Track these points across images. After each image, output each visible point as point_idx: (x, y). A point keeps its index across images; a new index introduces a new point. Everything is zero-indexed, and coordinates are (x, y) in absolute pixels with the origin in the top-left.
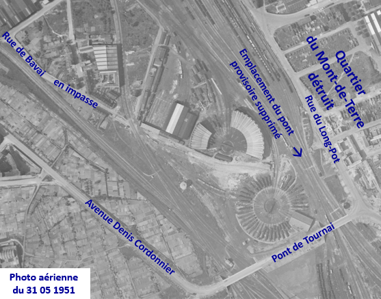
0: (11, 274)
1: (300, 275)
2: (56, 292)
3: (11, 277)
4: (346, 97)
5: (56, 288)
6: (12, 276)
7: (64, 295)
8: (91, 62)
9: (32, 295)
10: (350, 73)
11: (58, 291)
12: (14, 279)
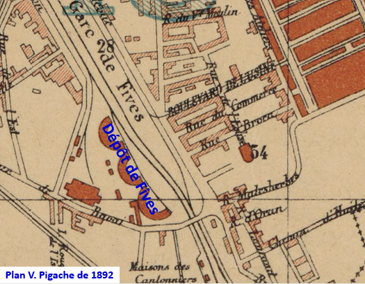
0: (7, 272)
1: (329, 147)
2: (94, 277)
3: (7, 275)
4: (265, 280)
5: (94, 273)
6: (8, 274)
7: (102, 280)
8: (134, 203)
9: (83, 280)
10: (109, 135)
11: (96, 275)
12: (10, 277)
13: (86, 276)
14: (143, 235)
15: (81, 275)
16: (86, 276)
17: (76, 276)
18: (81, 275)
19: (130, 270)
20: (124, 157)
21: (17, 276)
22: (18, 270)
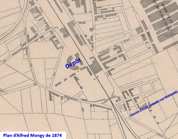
0: (4, 134)
2: (53, 136)
3: (4, 135)
5: (53, 134)
6: (4, 135)
9: (48, 138)
11: (54, 135)
12: (5, 136)
13: (49, 136)
14: (126, 51)
15: (47, 136)
16: (49, 136)
17: (45, 136)
18: (47, 136)
19: (79, 79)
20: (79, 60)
21: (8, 136)
22: (9, 133)
